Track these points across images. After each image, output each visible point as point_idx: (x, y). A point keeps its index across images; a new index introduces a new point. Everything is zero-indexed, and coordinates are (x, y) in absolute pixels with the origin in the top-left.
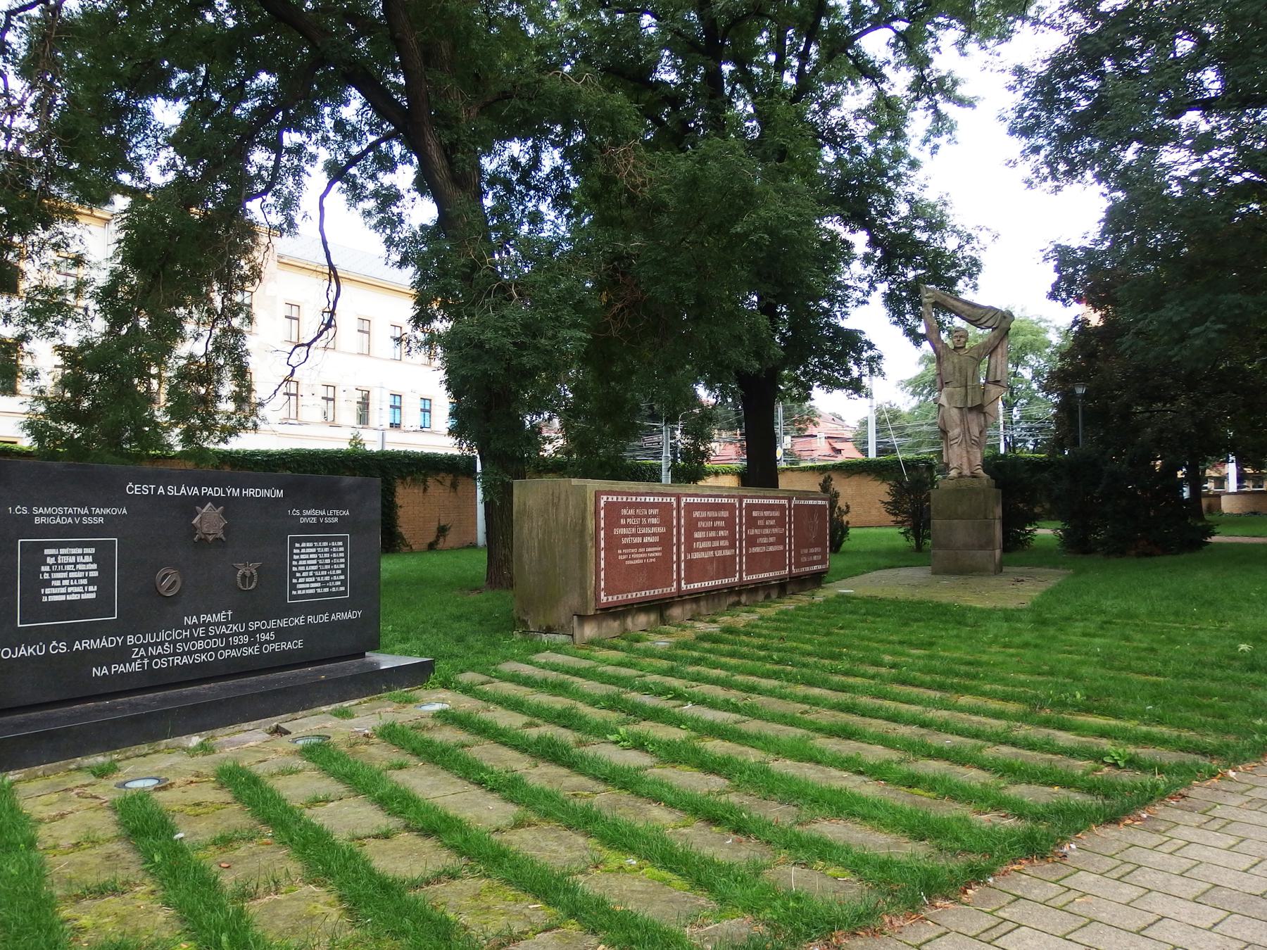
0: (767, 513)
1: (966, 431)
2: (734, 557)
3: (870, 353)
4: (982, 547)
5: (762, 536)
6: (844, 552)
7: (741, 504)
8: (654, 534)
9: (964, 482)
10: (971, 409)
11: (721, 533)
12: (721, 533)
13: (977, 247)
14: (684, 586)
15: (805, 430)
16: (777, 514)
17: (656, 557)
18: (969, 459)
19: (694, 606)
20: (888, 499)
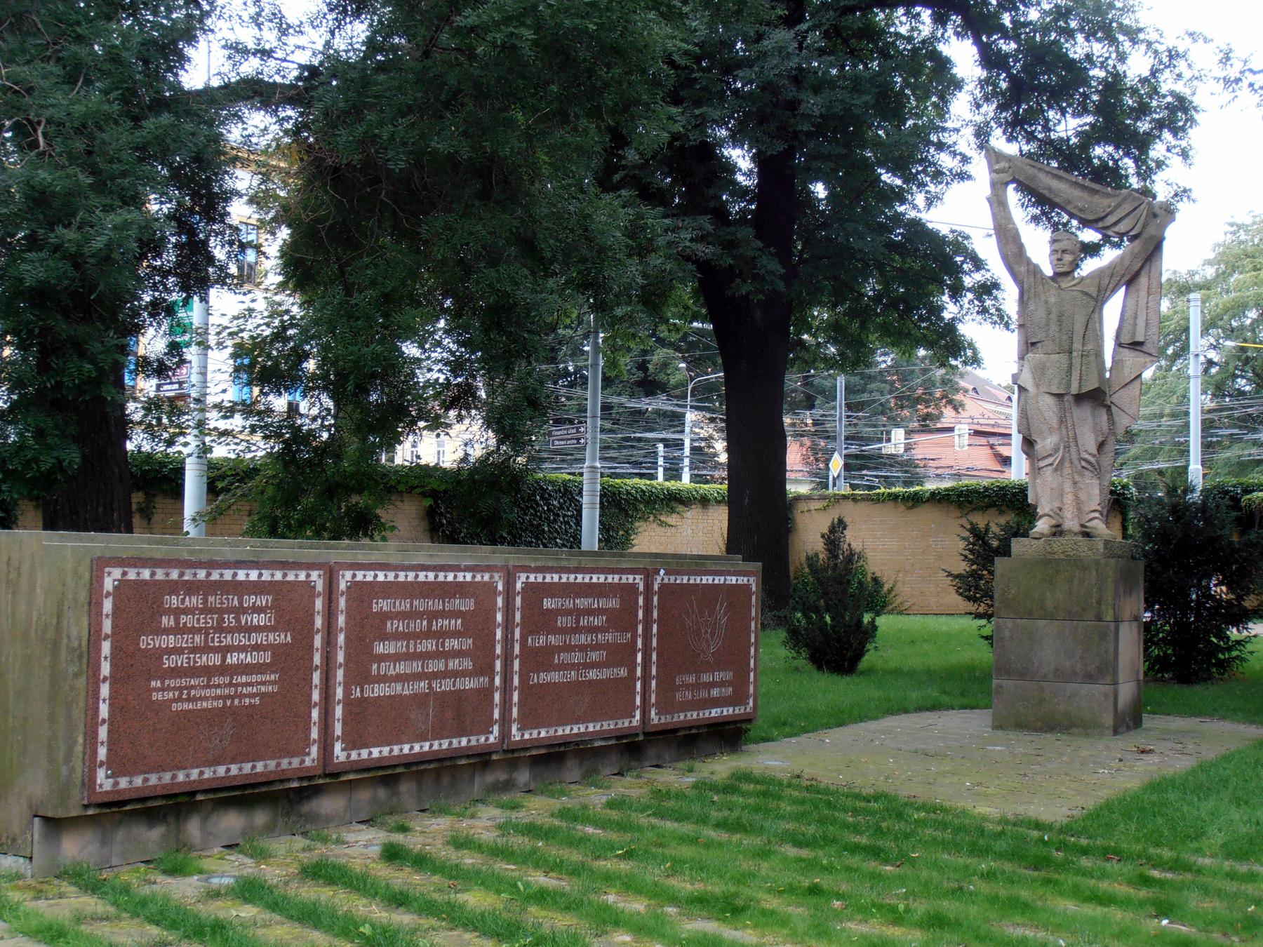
0: (582, 603)
1: (1071, 441)
2: (487, 692)
3: (978, 277)
4: (1089, 678)
5: (569, 648)
6: (869, 672)
7: (509, 584)
8: (257, 648)
9: (1059, 545)
10: (1080, 398)
11: (453, 644)
12: (453, 644)
13: (1187, 74)
14: (339, 752)
15: (938, 417)
16: (613, 603)
17: (263, 695)
18: (1077, 498)
19: (382, 793)
20: (962, 567)
